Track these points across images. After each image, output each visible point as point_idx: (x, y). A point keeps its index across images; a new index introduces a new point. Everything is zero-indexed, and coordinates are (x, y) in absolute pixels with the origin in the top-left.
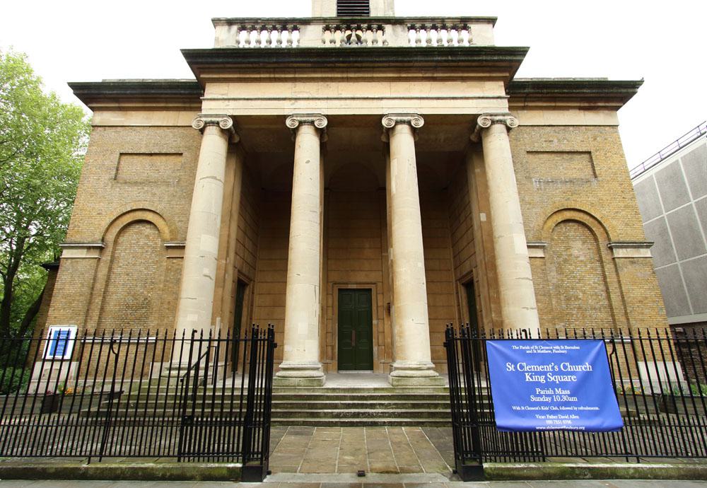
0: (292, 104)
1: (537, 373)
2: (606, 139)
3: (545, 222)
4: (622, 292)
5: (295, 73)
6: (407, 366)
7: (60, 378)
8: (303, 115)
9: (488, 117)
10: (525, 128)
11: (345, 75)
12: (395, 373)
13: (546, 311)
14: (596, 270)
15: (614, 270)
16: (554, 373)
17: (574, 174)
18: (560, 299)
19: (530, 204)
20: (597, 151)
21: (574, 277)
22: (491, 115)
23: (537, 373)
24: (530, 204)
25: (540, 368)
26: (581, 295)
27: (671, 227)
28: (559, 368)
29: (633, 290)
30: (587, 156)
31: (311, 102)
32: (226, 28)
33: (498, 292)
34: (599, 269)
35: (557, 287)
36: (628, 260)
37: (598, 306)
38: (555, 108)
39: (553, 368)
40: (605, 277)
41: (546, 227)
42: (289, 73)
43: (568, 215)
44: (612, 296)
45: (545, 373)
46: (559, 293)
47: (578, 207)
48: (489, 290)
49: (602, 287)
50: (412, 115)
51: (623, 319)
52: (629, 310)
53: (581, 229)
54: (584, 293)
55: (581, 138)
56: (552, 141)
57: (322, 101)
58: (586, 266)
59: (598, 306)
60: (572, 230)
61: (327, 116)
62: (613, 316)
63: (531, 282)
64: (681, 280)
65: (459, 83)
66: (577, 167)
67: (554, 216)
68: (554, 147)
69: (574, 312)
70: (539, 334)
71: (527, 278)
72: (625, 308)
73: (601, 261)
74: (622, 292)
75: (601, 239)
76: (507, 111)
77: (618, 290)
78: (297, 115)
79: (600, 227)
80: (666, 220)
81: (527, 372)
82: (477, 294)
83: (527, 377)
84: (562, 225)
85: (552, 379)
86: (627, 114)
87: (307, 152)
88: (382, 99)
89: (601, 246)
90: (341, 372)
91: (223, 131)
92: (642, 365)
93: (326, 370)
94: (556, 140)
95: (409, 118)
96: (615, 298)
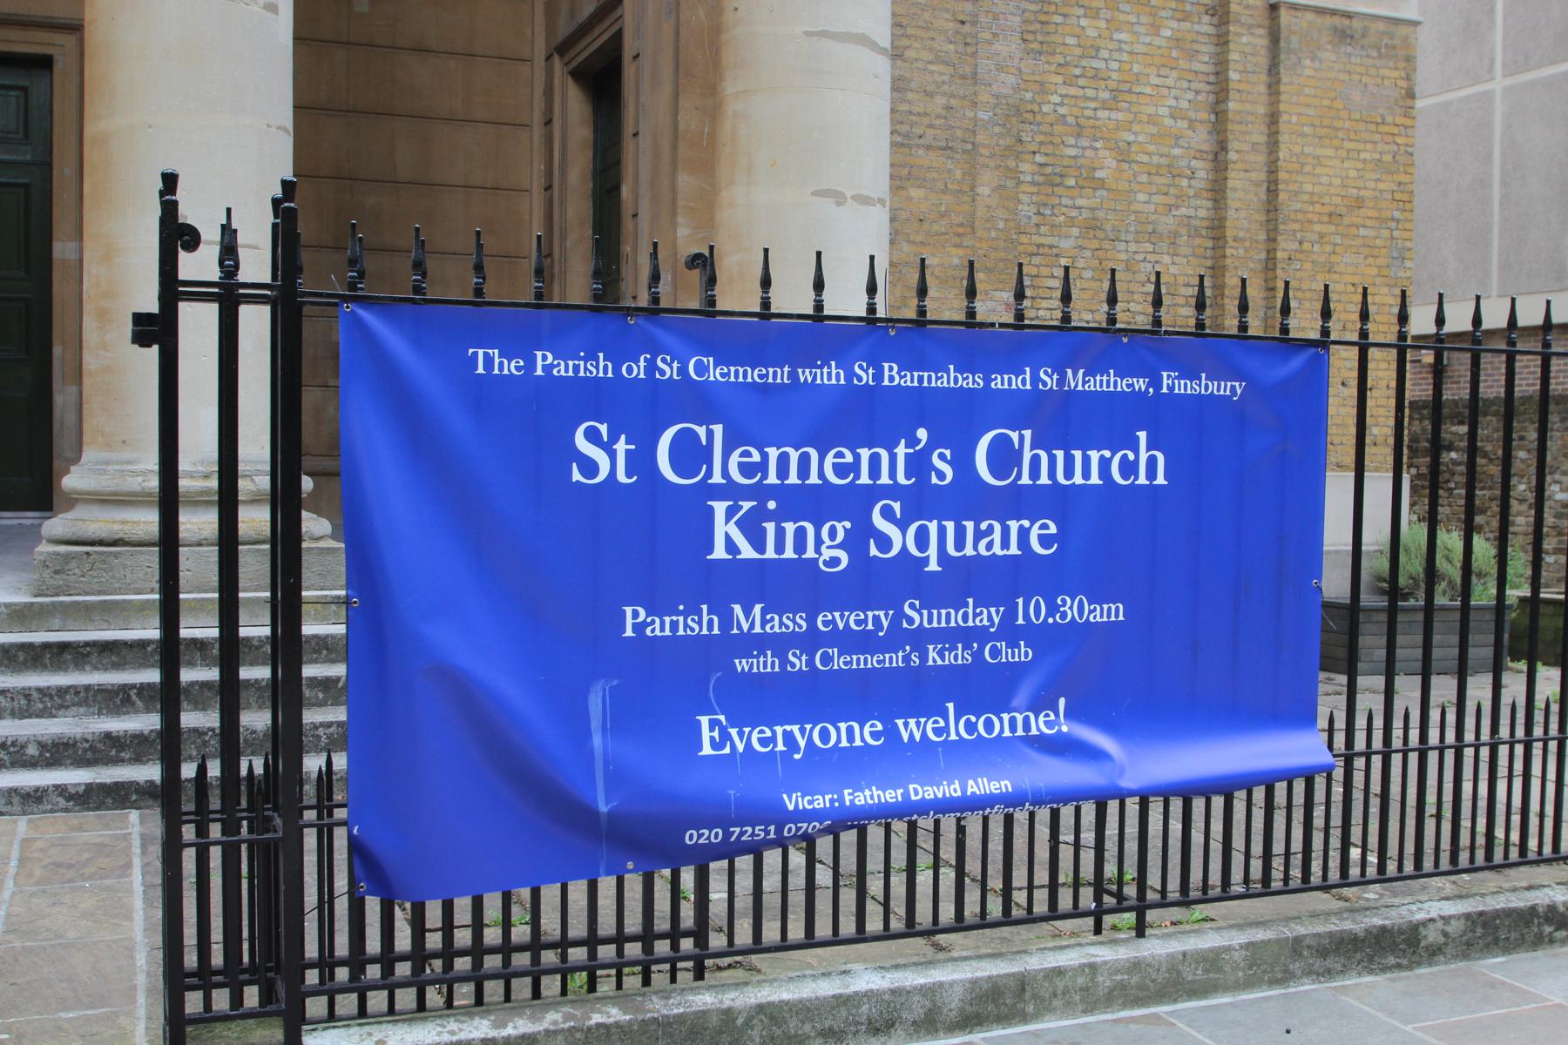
4: (1272, 169)
7: (184, 465)
12: (56, 525)
14: (1193, 54)
15: (1263, 61)
18: (1014, 174)
25: (825, 468)
26: (1107, 167)
28: (964, 463)
33: (713, 112)
34: (1207, 49)
35: (1018, 114)
36: (1328, 21)
37: (1167, 223)
39: (919, 464)
40: (1221, 91)
46: (1016, 149)
48: (676, 94)
49: (1201, 138)
52: (1285, 246)
54: (1124, 156)
58: (1155, 29)
59: (1167, 223)
63: (882, 67)
64: (1489, 155)
69: (1066, 244)
70: (872, 289)
71: (864, 40)
72: (1272, 240)
74: (1272, 169)
77: (1260, 159)
81: (730, 491)
82: (628, 130)
83: (724, 528)
85: (900, 540)
96: (1243, 188)
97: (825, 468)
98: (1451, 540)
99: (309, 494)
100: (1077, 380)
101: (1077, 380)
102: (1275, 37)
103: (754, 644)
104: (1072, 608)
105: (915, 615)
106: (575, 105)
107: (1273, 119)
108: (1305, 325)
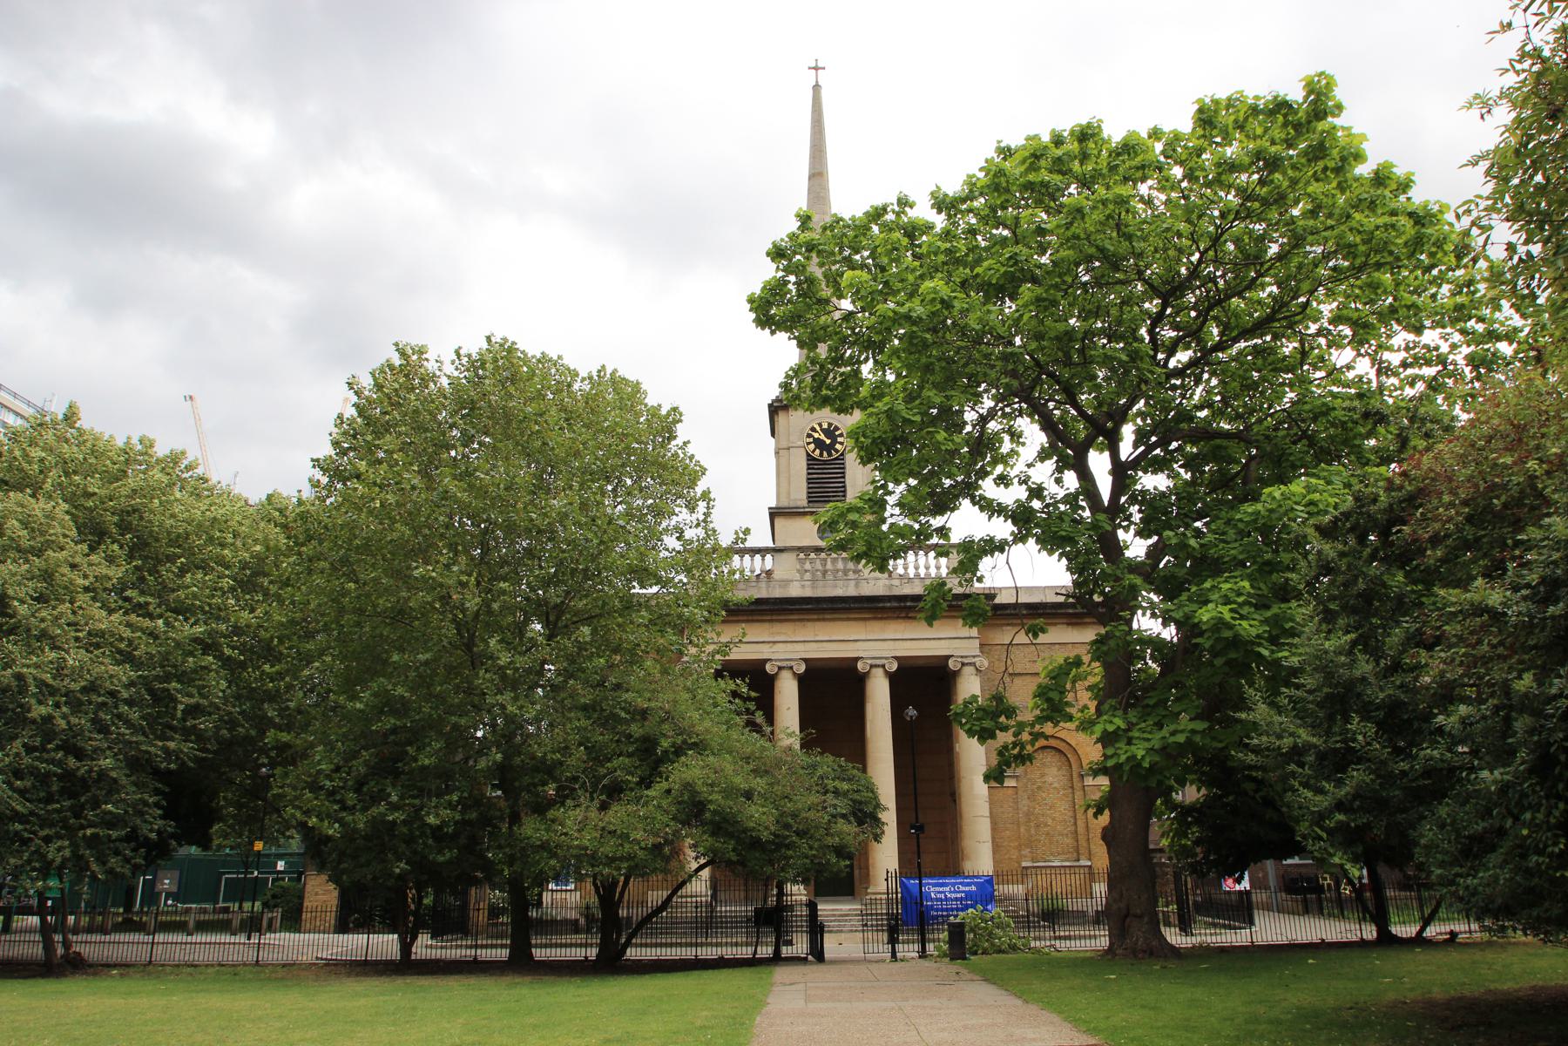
26: (1050, 822)
49: (1071, 814)
50: (886, 658)
51: (1085, 844)
52: (1091, 835)
53: (1058, 756)
54: (1054, 819)
61: (805, 660)
73: (1072, 787)
75: (1075, 767)
76: (977, 652)
87: (879, 696)
91: (886, 672)
95: (793, 663)
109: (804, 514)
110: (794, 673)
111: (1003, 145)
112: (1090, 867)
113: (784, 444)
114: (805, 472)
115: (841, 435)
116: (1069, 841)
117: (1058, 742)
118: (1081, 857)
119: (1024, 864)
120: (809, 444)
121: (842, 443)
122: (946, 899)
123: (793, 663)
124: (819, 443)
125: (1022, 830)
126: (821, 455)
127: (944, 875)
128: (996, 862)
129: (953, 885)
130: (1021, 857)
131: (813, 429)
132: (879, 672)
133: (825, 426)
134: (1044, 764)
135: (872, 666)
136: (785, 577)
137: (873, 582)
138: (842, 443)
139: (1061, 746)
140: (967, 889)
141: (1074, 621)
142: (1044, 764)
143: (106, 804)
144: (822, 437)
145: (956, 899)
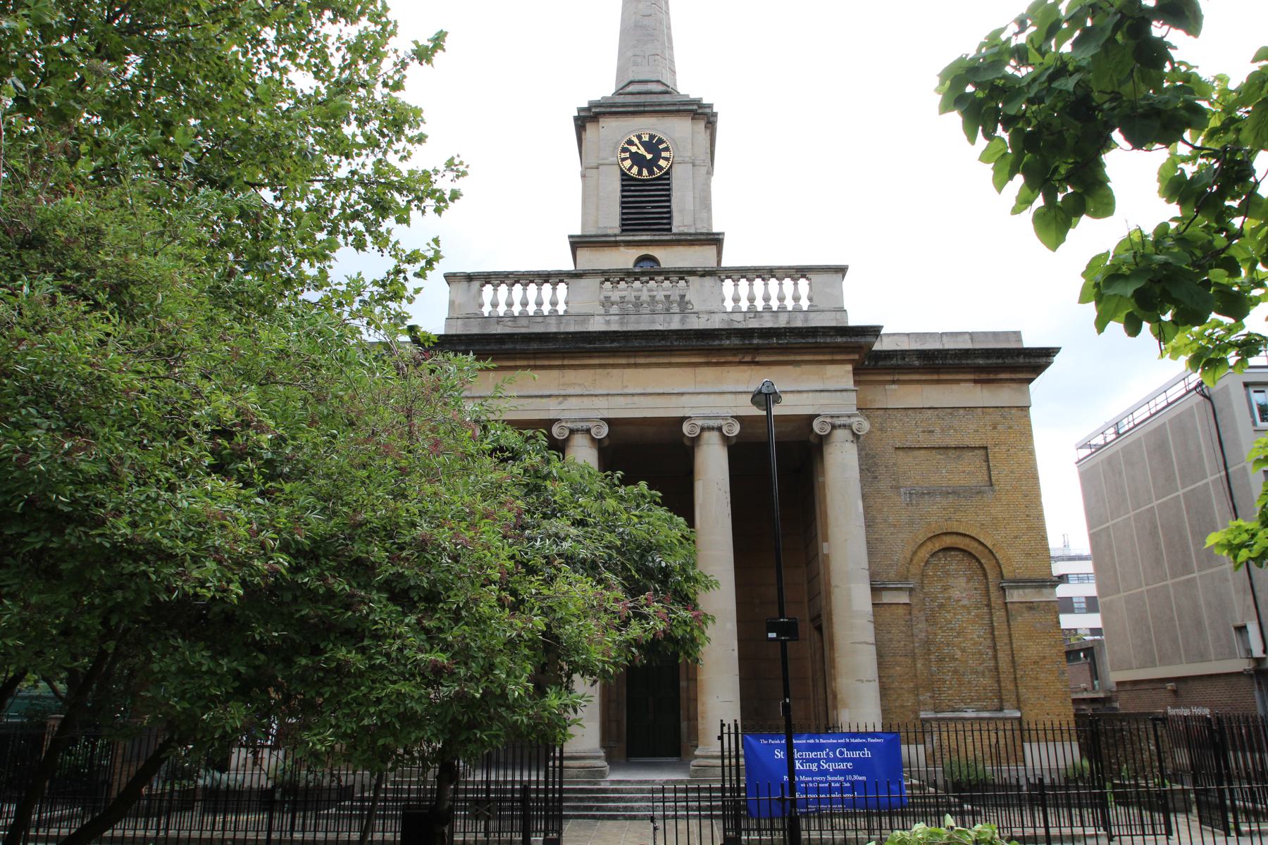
0: (560, 403)
1: (812, 761)
2: (1010, 428)
3: (915, 553)
5: (564, 358)
6: (710, 754)
8: (575, 420)
9: (828, 420)
10: (895, 412)
11: (632, 361)
12: (694, 762)
13: (906, 677)
15: (1005, 619)
16: (828, 760)
17: (959, 480)
19: (895, 526)
20: (996, 445)
21: (952, 629)
22: (832, 417)
23: (812, 761)
24: (895, 526)
25: (812, 755)
26: (958, 654)
27: (1162, 526)
28: (835, 754)
29: (1027, 646)
30: (982, 452)
31: (585, 399)
32: (464, 284)
37: (980, 669)
38: (938, 382)
39: (827, 754)
41: (916, 559)
42: (555, 358)
43: (948, 541)
44: (1000, 655)
45: (817, 760)
47: (961, 531)
49: (989, 642)
50: (724, 418)
51: (1011, 687)
52: (1019, 673)
54: (963, 651)
55: (974, 427)
56: (933, 432)
57: (601, 398)
58: (969, 613)
60: (955, 564)
61: (609, 422)
62: (999, 682)
65: (790, 368)
66: (967, 469)
67: (929, 543)
68: (937, 440)
69: (948, 678)
71: (866, 643)
72: (1015, 671)
73: (989, 605)
76: (854, 410)
77: (1008, 647)
78: (567, 421)
79: (991, 557)
80: (1182, 501)
84: (941, 555)
85: (826, 766)
86: (1040, 387)
88: (682, 394)
89: (991, 585)
90: (633, 760)
91: (726, 439)
92: (1027, 746)
93: (610, 758)
94: (938, 430)
97: (812, 755)
98: (1013, 768)
99: (1107, 144)
100: (853, 740)
101: (853, 740)
102: (1007, 610)
103: (803, 782)
104: (856, 777)
105: (829, 778)
106: (816, 634)
107: (1010, 635)
108: (895, 729)
109: (616, 244)
110: (593, 439)
111: (710, 622)
112: (1020, 720)
113: (592, 161)
114: (618, 194)
115: (667, 149)
116: (987, 681)
117: (967, 540)
118: (1006, 704)
119: (923, 715)
120: (623, 160)
121: (667, 159)
122: (824, 773)
123: (590, 425)
124: (637, 159)
125: (919, 665)
126: (640, 173)
127: (817, 734)
128: (885, 711)
129: (833, 747)
130: (919, 705)
131: (630, 143)
132: (712, 439)
133: (646, 138)
134: (947, 574)
135: (703, 429)
136: (583, 311)
137: (706, 317)
138: (667, 159)
139: (972, 547)
140: (856, 754)
141: (984, 376)
142: (947, 574)
143: (306, 666)
144: (642, 151)
145: (836, 772)
